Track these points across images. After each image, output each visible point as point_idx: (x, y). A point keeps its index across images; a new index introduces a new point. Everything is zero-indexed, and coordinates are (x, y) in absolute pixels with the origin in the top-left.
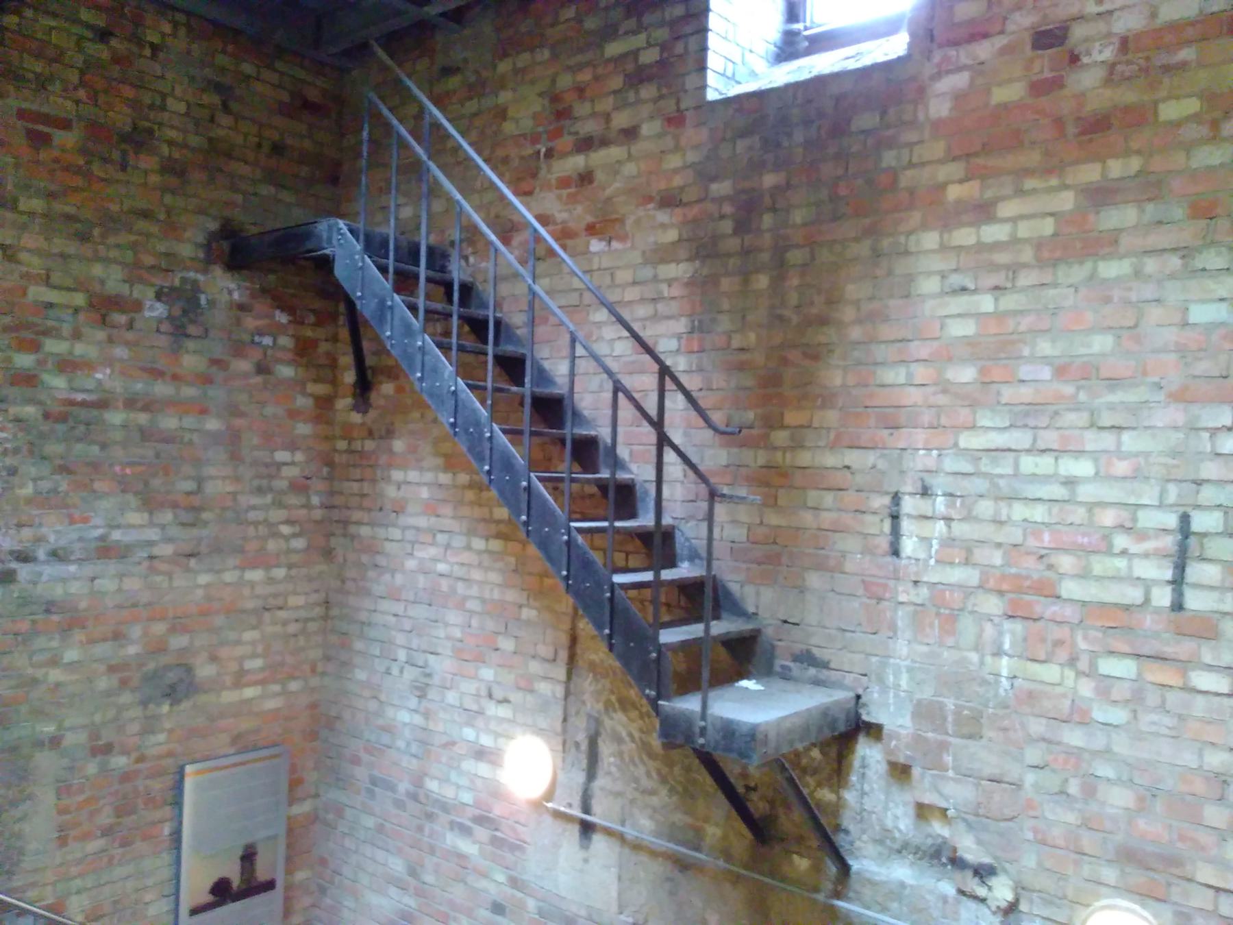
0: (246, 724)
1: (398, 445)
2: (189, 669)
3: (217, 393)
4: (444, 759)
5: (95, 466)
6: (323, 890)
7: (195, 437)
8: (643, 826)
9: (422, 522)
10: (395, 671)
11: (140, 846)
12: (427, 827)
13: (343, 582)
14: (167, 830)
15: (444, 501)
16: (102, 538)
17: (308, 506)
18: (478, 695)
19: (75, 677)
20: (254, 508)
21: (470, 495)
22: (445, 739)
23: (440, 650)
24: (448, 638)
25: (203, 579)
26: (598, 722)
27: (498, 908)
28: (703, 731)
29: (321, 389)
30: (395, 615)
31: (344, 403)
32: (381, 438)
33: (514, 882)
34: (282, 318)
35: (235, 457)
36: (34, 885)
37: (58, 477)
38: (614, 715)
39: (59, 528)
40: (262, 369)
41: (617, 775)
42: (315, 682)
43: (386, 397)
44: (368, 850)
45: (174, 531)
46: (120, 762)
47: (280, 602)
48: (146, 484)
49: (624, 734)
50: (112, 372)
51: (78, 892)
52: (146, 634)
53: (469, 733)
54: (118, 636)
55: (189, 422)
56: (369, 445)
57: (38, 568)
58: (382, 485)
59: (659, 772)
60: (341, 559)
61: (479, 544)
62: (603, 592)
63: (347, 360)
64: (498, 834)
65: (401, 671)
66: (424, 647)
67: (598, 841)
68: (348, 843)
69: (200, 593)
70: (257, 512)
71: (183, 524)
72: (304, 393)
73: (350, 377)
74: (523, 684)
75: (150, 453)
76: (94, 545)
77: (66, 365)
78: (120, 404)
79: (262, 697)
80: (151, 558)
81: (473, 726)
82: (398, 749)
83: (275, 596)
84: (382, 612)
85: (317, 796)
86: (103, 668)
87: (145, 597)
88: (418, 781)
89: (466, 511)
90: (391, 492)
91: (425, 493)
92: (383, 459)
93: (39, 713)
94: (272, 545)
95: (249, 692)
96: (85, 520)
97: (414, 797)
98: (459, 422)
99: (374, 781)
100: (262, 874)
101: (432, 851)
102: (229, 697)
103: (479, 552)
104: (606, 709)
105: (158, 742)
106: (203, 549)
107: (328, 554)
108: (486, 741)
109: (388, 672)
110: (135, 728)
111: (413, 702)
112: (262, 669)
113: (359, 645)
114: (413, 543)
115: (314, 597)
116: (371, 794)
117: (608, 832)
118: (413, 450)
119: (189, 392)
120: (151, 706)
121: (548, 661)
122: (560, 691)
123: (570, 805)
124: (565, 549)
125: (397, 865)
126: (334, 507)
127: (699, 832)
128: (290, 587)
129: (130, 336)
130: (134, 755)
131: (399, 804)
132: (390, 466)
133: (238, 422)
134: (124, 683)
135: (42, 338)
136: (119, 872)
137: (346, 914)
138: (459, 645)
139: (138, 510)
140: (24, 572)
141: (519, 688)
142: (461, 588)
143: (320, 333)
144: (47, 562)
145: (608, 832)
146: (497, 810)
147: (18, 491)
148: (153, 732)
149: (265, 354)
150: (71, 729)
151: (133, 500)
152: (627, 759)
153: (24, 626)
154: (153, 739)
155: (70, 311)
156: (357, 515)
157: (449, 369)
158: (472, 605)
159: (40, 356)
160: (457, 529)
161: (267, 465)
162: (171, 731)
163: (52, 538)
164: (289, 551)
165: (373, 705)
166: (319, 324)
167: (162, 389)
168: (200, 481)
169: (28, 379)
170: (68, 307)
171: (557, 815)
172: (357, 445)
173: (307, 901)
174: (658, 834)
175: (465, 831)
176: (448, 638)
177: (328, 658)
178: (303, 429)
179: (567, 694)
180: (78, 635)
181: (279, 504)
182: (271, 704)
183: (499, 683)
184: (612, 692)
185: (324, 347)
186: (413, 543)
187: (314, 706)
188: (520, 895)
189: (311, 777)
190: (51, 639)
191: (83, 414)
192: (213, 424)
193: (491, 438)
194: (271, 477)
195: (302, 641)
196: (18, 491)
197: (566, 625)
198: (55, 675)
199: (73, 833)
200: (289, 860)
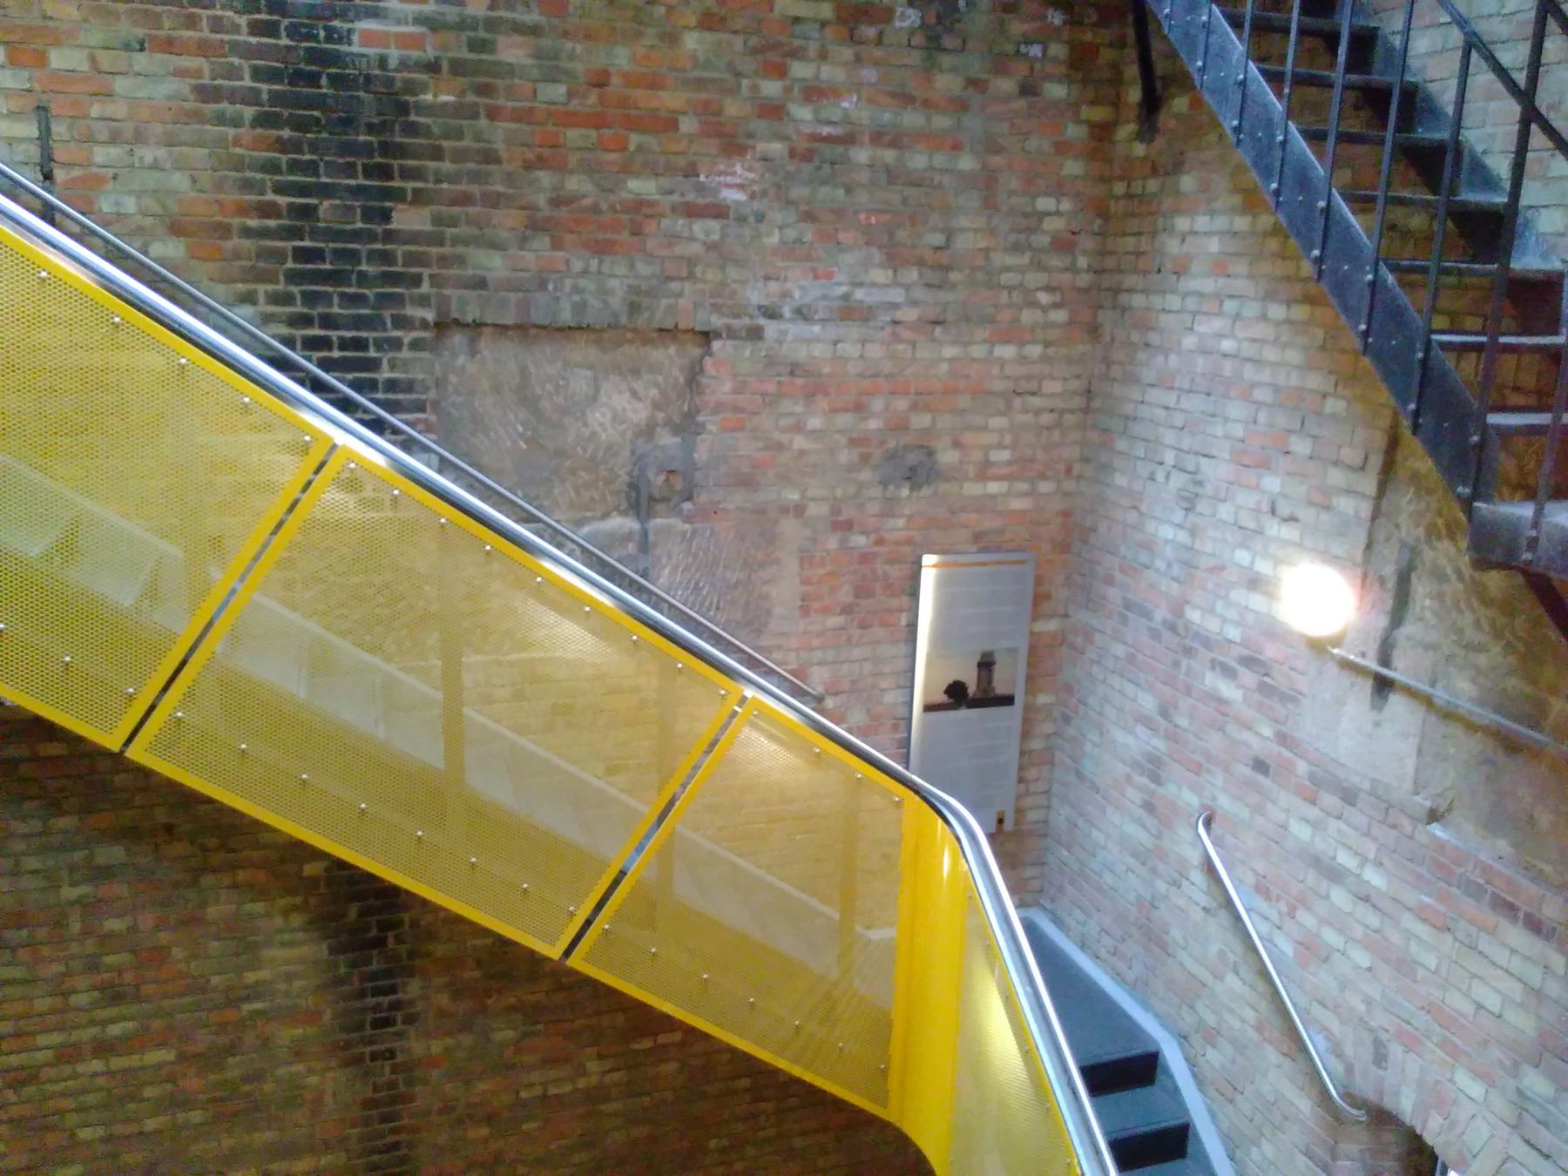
0: (989, 523)
1: (1187, 182)
2: (931, 453)
3: (973, 123)
4: (1210, 586)
5: (839, 213)
6: (1067, 719)
7: (947, 180)
8: (1462, 690)
9: (1208, 285)
10: (1160, 476)
11: (879, 632)
12: (1184, 662)
13: (1108, 366)
14: (904, 621)
15: (1237, 254)
16: (846, 297)
17: (1072, 269)
18: (1258, 511)
19: (818, 446)
20: (1008, 269)
21: (1273, 244)
22: (1212, 562)
23: (1214, 452)
24: (1226, 437)
25: (949, 352)
26: (1414, 551)
27: (1261, 766)
28: (1533, 544)
29: (1099, 114)
30: (1167, 408)
31: (1127, 130)
32: (1167, 174)
33: (1283, 739)
34: (1056, 18)
35: (989, 204)
36: (779, 647)
37: (802, 225)
38: (1438, 544)
39: (802, 283)
40: (1028, 89)
41: (1433, 621)
42: (1069, 485)
43: (1179, 117)
44: (1116, 681)
45: (919, 293)
46: (859, 541)
47: (1033, 386)
48: (891, 235)
49: (1449, 570)
50: (859, 99)
51: (819, 664)
52: (887, 408)
53: (1242, 556)
54: (859, 408)
55: (940, 160)
56: (1153, 185)
57: (783, 326)
58: (1163, 237)
59: (1493, 624)
60: (1108, 338)
61: (1277, 311)
62: (1413, 350)
63: (1132, 71)
64: (1266, 679)
65: (1167, 478)
66: (1196, 448)
67: (1396, 701)
68: (1095, 670)
69: (944, 367)
70: (1011, 275)
71: (929, 285)
72: (1078, 121)
73: (1134, 95)
74: (1317, 497)
75: (895, 199)
76: (836, 304)
77: (814, 93)
78: (866, 139)
79: (1008, 494)
80: (896, 323)
81: (1248, 548)
82: (1157, 571)
83: (1028, 378)
84: (1150, 404)
85: (1066, 616)
86: (843, 440)
87: (887, 367)
88: (1178, 608)
89: (1266, 267)
90: (1173, 246)
91: (1214, 245)
92: (1167, 203)
93: (785, 479)
94: (1027, 316)
95: (994, 487)
96: (829, 276)
97: (1173, 628)
98: (1246, 126)
99: (1128, 606)
100: (1000, 688)
101: (1188, 691)
102: (972, 489)
103: (1278, 323)
104: (1429, 535)
105: (896, 526)
106: (950, 316)
107: (1094, 330)
108: (1263, 567)
109: (1152, 478)
110: (873, 508)
111: (1178, 516)
112: (1009, 463)
113: (1121, 445)
114: (1195, 314)
115: (1075, 385)
116: (1124, 620)
117: (1410, 692)
118: (1205, 187)
119: (942, 122)
120: (891, 488)
121: (1351, 468)
122: (1366, 509)
123: (1363, 655)
124: (1367, 293)
125: (1148, 703)
126: (1104, 271)
127: (1540, 707)
128: (1046, 369)
129: (878, 53)
130: (873, 537)
131: (1155, 634)
132: (1176, 211)
133: (996, 160)
134: (865, 458)
135: (788, 61)
136: (857, 653)
137: (1088, 747)
138: (1241, 445)
139: (881, 266)
140: (771, 329)
141: (1311, 504)
142: (1249, 372)
143: (1105, 35)
144: (791, 320)
145: (1410, 692)
146: (1270, 652)
147: (766, 240)
148: (893, 516)
149: (1032, 69)
150: (813, 499)
151: (878, 256)
152: (1448, 603)
153: (771, 387)
154: (891, 523)
155: (817, 26)
156: (1130, 280)
157: (1238, 46)
158: (1261, 394)
159: (787, 82)
160: (1251, 294)
161: (1026, 215)
162: (910, 518)
163: (797, 294)
164: (1048, 325)
165: (1132, 517)
166: (1103, 22)
167: (912, 119)
168: (950, 234)
169: (773, 111)
170: (815, 20)
171: (1346, 665)
172: (1137, 188)
173: (1048, 728)
174: (1481, 702)
175: (1228, 672)
176: (1226, 437)
177: (1086, 460)
178: (1073, 167)
179: (1376, 515)
180: (822, 403)
181: (1040, 267)
182: (1018, 504)
183: (1285, 496)
184: (1440, 513)
185: (1107, 55)
186: (1195, 314)
187: (1066, 514)
188: (1287, 754)
189: (1061, 594)
190: (796, 403)
191: (827, 150)
192: (966, 163)
193: (1284, 143)
194: (1031, 230)
195: (1056, 435)
196: (766, 240)
197: (1385, 422)
198: (799, 442)
199: (816, 605)
200: (1030, 679)
